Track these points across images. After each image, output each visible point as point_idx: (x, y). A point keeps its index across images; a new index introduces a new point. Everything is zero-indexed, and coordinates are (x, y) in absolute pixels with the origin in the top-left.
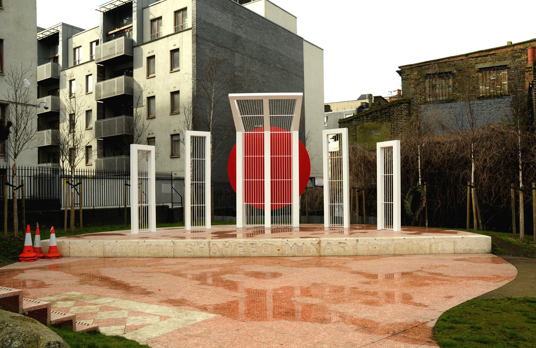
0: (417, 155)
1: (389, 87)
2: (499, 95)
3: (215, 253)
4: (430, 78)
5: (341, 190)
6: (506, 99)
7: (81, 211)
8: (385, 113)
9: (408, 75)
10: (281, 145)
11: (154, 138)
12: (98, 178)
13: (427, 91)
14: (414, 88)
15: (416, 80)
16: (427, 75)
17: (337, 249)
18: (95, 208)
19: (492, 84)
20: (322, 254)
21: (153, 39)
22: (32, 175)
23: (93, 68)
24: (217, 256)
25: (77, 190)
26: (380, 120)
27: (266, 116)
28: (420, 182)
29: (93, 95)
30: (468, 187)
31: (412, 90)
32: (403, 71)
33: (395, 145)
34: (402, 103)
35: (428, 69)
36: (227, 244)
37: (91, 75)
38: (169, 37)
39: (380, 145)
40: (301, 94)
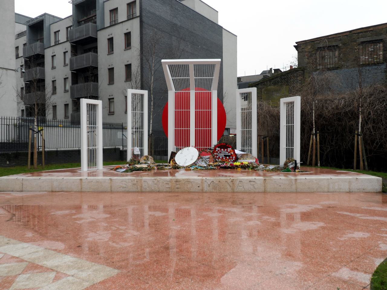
0: (312, 110)
1: (287, 60)
2: (376, 63)
3: (146, 189)
4: (320, 51)
5: (250, 138)
6: (382, 67)
7: (43, 153)
8: (284, 79)
9: (303, 48)
10: (203, 102)
11: (113, 98)
12: (70, 127)
13: (318, 61)
14: (308, 59)
15: (309, 52)
16: (318, 48)
17: (248, 187)
18: (59, 149)
19: (371, 54)
20: (236, 191)
21: (112, 24)
22: (10, 124)
23: (68, 46)
24: (147, 191)
25: (41, 135)
26: (280, 84)
27: (192, 78)
28: (314, 131)
29: (68, 67)
30: (356, 135)
31: (306, 60)
32: (299, 46)
33: (297, 100)
34: (298, 71)
35: (319, 43)
36: (156, 182)
37: (67, 52)
38: (124, 23)
39: (283, 101)
40: (220, 60)
